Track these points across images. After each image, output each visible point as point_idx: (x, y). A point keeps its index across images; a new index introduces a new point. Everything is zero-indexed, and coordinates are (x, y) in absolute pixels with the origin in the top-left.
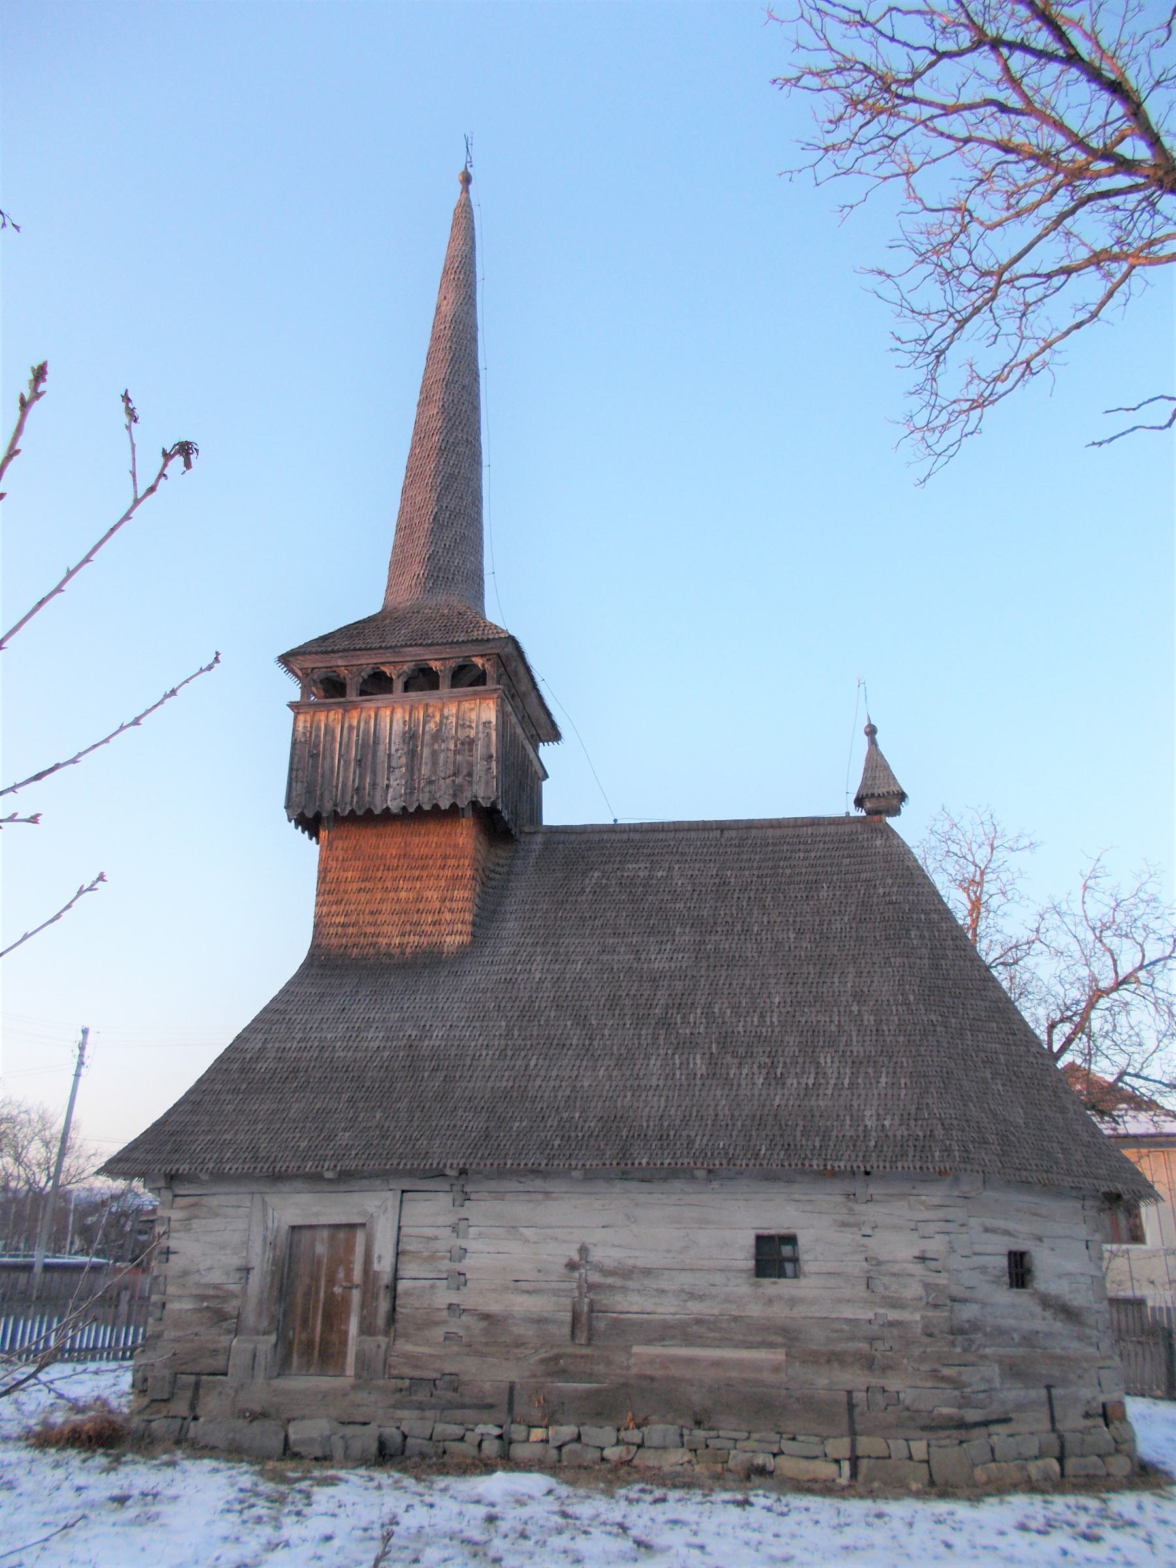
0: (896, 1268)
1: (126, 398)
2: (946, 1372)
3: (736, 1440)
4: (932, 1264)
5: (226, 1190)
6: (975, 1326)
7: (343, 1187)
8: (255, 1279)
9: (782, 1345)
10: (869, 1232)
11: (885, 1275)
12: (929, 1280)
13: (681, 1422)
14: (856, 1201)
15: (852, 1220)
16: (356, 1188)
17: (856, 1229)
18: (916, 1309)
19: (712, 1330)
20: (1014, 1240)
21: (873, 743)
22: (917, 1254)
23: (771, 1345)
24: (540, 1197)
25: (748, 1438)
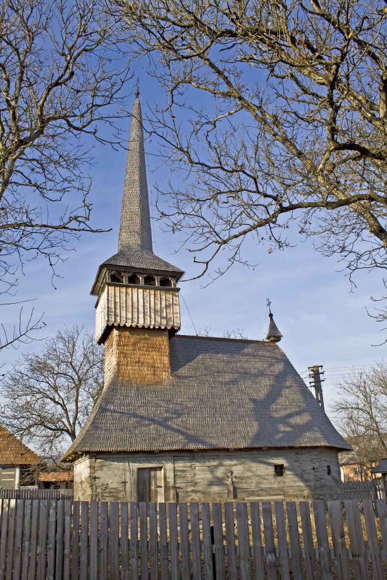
0: (308, 472)
1: (111, 229)
2: (321, 497)
5: (228, 454)
6: (324, 485)
8: (128, 485)
14: (298, 454)
21: (272, 319)
23: (280, 495)
24: (215, 457)
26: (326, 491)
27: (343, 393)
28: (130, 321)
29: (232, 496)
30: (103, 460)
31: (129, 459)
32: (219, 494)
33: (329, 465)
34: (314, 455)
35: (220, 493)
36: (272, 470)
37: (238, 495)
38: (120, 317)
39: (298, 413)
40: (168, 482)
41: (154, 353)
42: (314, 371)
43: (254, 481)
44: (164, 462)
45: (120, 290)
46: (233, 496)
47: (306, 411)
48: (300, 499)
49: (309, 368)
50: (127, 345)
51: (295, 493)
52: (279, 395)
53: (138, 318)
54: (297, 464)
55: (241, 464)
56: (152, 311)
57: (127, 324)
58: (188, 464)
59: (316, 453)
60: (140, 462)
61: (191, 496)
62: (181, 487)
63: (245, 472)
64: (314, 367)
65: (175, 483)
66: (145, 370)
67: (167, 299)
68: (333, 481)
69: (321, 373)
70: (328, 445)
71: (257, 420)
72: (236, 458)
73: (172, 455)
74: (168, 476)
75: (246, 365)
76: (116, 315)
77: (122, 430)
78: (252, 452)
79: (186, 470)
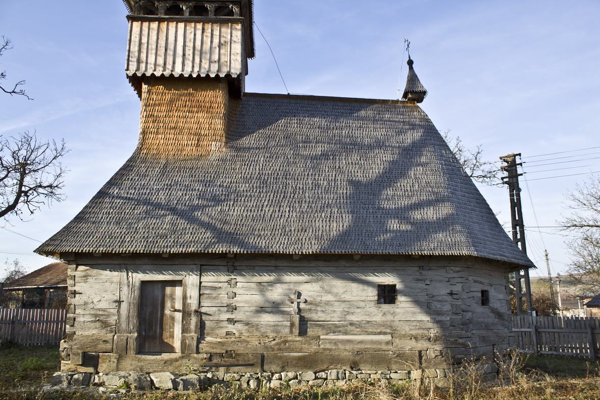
0: (440, 298)
2: (460, 341)
3: (370, 374)
4: (455, 296)
6: (470, 321)
7: (169, 263)
8: (124, 306)
9: (389, 333)
10: (429, 283)
11: (435, 301)
12: (453, 303)
13: (344, 368)
14: (423, 269)
15: (420, 277)
16: (176, 263)
17: (423, 282)
18: (448, 315)
19: (357, 328)
20: (483, 286)
21: (411, 68)
22: (449, 292)
23: (385, 333)
24: (273, 268)
25: (376, 374)
26: (474, 332)
27: (577, 207)
28: (161, 69)
29: (296, 331)
30: (88, 268)
31: (129, 267)
32: (276, 327)
33: (485, 288)
34: (452, 272)
35: (277, 326)
36: (372, 293)
37: (308, 330)
38: (147, 63)
39: (429, 203)
40: (189, 305)
41: (200, 115)
42: (507, 162)
43: (339, 308)
44: (183, 273)
45: (149, 25)
46: (298, 331)
47: (448, 201)
48: (421, 342)
49: (501, 158)
50: (159, 105)
51: (414, 332)
52: (403, 174)
53: (174, 63)
54: (421, 285)
55: (317, 281)
56: (197, 53)
57: (155, 73)
58: (224, 278)
59: (458, 269)
60: (144, 272)
61: (226, 327)
62: (210, 313)
63: (322, 294)
64: (509, 156)
65: (200, 306)
66: (184, 139)
67: (222, 34)
68: (492, 315)
69: (518, 164)
70: (475, 254)
71: (352, 212)
72: (308, 272)
73: (199, 262)
74: (188, 296)
75: (357, 133)
76: (139, 61)
77: (118, 223)
78: (332, 261)
79: (220, 288)
